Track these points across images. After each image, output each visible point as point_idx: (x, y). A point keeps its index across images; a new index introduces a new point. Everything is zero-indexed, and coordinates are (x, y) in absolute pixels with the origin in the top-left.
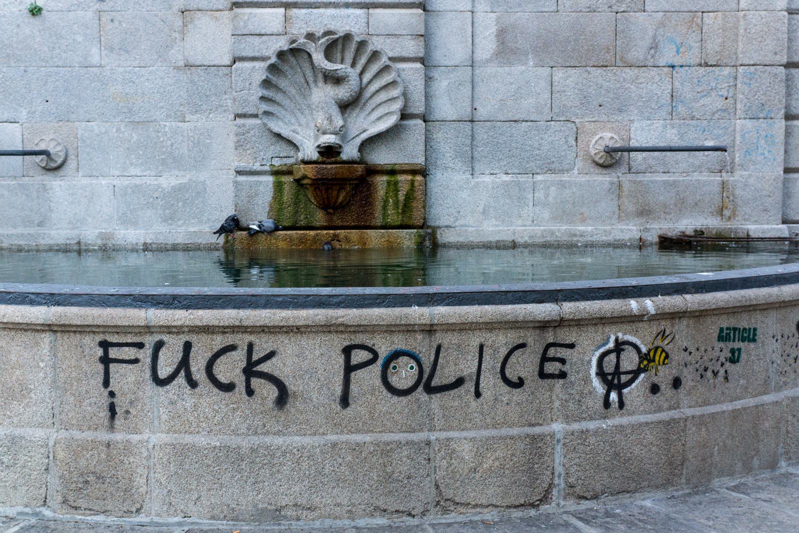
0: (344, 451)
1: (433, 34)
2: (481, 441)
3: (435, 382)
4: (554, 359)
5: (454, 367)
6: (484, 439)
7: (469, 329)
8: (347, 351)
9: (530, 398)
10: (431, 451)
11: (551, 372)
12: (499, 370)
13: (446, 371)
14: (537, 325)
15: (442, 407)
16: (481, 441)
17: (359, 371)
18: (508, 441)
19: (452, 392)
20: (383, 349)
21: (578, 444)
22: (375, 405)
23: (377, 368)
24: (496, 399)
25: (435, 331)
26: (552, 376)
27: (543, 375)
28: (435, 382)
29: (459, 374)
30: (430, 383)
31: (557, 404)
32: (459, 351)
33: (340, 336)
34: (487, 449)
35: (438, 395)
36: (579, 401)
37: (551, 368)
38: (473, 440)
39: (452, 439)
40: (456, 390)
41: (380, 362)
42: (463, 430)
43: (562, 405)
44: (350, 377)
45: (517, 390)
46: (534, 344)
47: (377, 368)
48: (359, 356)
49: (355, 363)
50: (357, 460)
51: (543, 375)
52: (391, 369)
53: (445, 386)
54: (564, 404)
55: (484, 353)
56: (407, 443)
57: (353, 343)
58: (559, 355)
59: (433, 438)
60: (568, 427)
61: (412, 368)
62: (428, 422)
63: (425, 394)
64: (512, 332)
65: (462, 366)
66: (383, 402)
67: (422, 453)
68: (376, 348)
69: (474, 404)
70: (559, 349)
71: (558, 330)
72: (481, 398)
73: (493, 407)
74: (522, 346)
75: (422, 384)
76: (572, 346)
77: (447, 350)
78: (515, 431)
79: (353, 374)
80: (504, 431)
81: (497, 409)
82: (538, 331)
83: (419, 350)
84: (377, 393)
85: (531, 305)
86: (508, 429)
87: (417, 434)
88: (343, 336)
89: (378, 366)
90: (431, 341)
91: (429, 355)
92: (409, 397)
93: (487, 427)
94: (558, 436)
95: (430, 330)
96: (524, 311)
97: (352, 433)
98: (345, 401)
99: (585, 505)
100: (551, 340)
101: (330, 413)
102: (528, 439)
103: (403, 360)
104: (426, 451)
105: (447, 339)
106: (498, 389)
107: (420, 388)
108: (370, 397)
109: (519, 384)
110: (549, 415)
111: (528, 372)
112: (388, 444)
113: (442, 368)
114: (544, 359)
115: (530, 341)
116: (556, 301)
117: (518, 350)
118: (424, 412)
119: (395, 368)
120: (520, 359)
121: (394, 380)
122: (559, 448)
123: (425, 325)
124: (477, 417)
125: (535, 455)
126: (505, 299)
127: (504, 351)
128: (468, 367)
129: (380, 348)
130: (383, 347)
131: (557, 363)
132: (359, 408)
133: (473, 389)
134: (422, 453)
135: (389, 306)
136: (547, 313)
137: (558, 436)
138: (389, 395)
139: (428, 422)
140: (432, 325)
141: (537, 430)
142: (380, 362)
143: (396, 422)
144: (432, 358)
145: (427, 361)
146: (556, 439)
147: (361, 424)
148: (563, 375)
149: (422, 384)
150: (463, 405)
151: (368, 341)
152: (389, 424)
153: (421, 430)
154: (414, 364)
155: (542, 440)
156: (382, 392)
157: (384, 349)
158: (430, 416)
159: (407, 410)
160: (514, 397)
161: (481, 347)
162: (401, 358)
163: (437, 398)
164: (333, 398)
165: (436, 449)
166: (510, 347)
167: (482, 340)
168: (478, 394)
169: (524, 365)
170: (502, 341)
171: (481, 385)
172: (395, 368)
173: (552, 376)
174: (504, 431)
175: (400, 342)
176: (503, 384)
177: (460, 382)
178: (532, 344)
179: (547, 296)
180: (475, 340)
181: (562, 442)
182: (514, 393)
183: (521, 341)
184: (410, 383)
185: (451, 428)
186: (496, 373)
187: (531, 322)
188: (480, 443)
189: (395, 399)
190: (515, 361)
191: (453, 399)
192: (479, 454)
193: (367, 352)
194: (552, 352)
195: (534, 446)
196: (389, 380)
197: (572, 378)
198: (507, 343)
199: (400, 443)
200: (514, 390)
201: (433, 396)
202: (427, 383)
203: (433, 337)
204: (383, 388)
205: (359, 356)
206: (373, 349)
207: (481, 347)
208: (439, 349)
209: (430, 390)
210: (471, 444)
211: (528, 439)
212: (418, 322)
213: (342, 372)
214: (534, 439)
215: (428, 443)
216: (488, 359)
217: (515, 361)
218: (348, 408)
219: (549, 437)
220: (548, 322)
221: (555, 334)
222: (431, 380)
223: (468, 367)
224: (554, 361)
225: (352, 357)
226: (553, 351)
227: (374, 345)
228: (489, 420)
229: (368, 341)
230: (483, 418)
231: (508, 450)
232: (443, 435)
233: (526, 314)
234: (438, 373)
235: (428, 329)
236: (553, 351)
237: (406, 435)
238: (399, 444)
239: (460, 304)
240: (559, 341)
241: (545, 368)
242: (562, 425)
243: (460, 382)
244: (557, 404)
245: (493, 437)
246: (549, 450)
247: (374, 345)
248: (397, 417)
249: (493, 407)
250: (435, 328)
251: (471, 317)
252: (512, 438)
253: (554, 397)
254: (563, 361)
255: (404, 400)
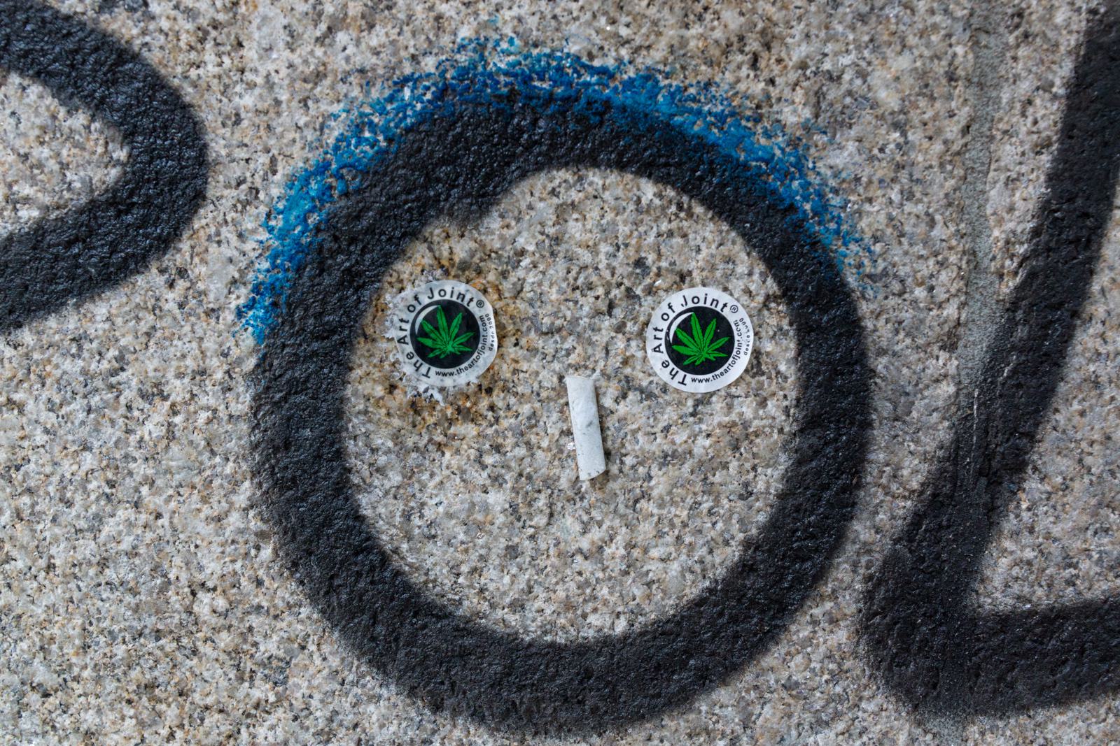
1: (94, 302)
20: (269, 53)
23: (187, 336)
41: (230, 246)
52: (385, 371)
75: (846, 585)
84: (212, 677)
91: (970, 159)
103: (574, 225)
107: (822, 637)
119: (448, 336)
121: (442, 513)
142: (230, 246)
149: (846, 585)
154: (738, 288)
156: (278, 670)
162: (536, 198)
184: (668, 560)
196: (378, 505)
204: (289, 619)
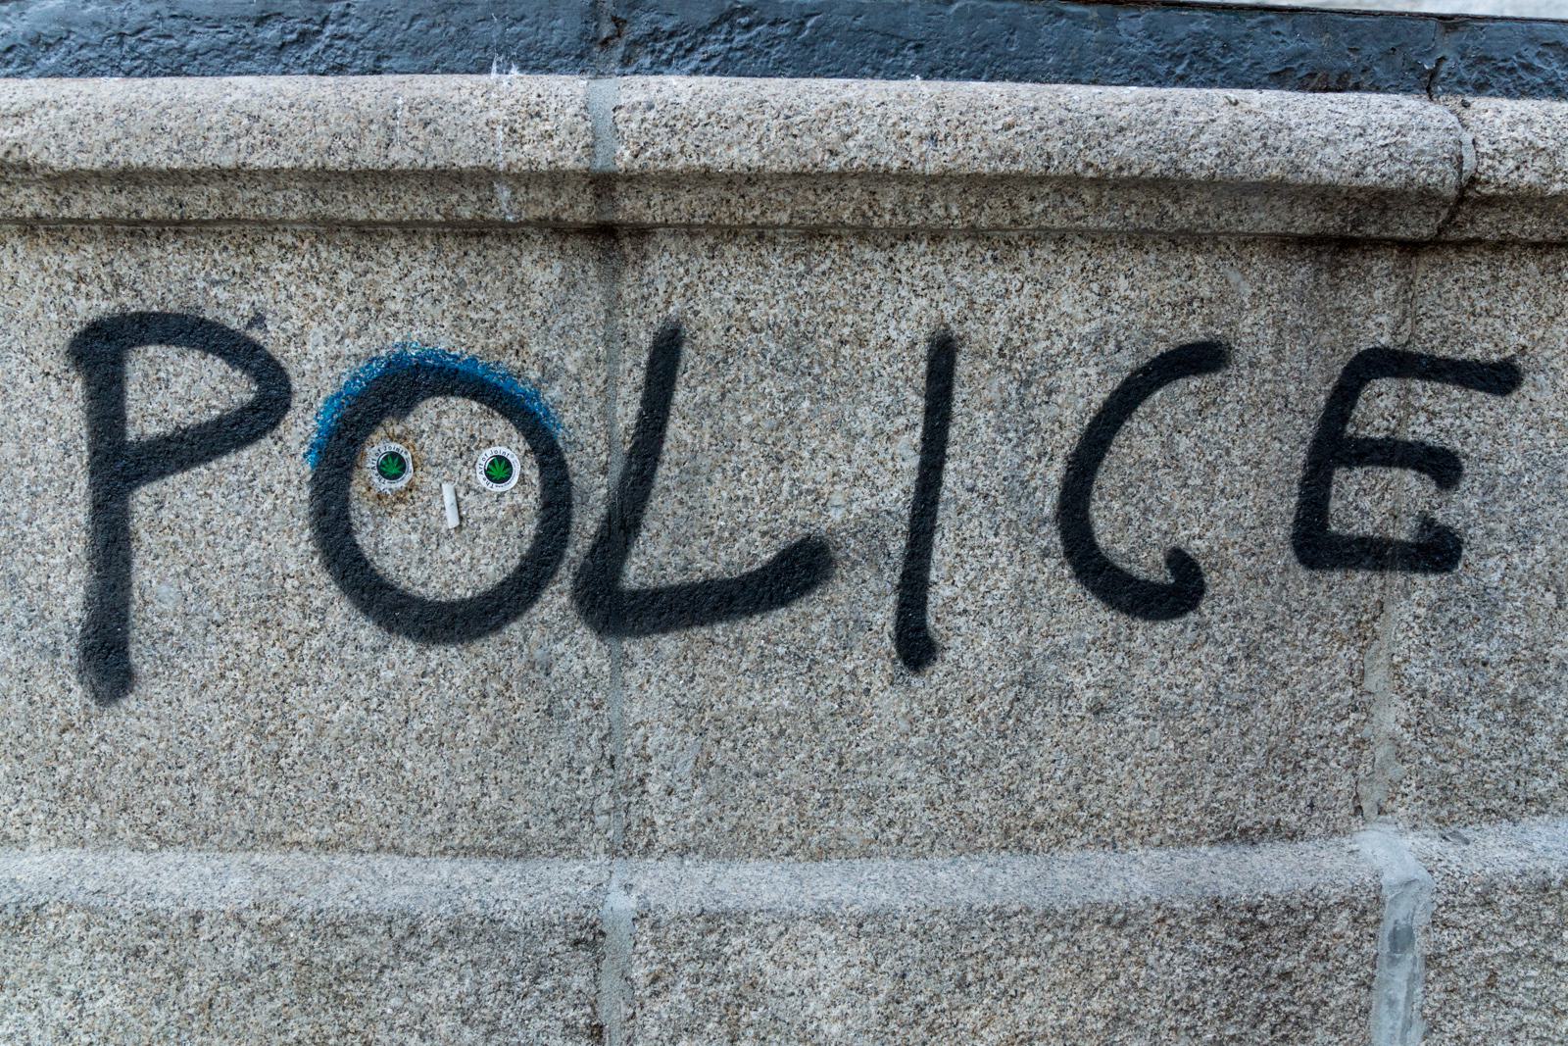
0: (76, 957)
2: (925, 933)
3: (647, 564)
4: (1393, 453)
5: (764, 476)
6: (942, 925)
7: (863, 233)
8: (101, 352)
9: (1237, 681)
10: (609, 982)
11: (1365, 528)
12: (1049, 504)
13: (716, 495)
14: (1305, 222)
15: (691, 715)
16: (925, 933)
17: (177, 479)
18: (1094, 938)
19: (756, 628)
21: (1514, 957)
22: (282, 691)
23: (283, 463)
24: (1026, 681)
25: (642, 232)
26: (1374, 553)
27: (1318, 544)
28: (647, 564)
29: (797, 521)
30: (617, 572)
31: (1391, 717)
32: (796, 372)
33: (52, 260)
34: (962, 985)
35: (669, 644)
36: (1520, 704)
37: (1370, 502)
38: (871, 925)
39: (741, 918)
40: (781, 616)
41: (300, 428)
42: (823, 854)
43: (1419, 724)
44: (125, 515)
45: (1163, 630)
46: (1278, 352)
47: (283, 463)
48: (173, 389)
49: (153, 429)
50: (160, 1016)
51: (1318, 544)
53: (709, 586)
54: (1432, 719)
55: (960, 393)
56: (456, 931)
57: (134, 306)
58: (1419, 430)
59: (622, 904)
60: (1452, 852)
61: (500, 469)
62: (605, 802)
63: (584, 635)
64: (1142, 265)
65: (816, 473)
66: (331, 672)
67: (550, 996)
68: (271, 338)
69: (891, 704)
70: (1423, 391)
71: (1426, 272)
72: (938, 671)
73: (1011, 724)
74: (1201, 358)
76: (1500, 378)
77: (719, 365)
78: (1137, 875)
79: (142, 499)
80: (1080, 875)
81: (1036, 738)
82: (1303, 273)
83: (544, 362)
84: (292, 617)
85: (1271, 95)
86: (1098, 857)
87: (539, 868)
88: (72, 263)
89: (287, 453)
90: (613, 306)
92: (489, 649)
93: (969, 841)
94: (1396, 914)
95: (602, 219)
96: (1225, 117)
97: (163, 843)
98: (107, 656)
99: (698, 56)
100: (1379, 333)
101: (30, 726)
102: (1215, 931)
103: (445, 418)
104: (578, 981)
105: (723, 296)
106: (1039, 619)
107: (556, 600)
108: (251, 643)
109: (1176, 591)
110: (1344, 784)
111: (1233, 523)
112: (336, 930)
113: (691, 476)
114: (1335, 447)
115: (1251, 330)
116: (1428, 84)
117: (1179, 386)
118: (579, 742)
120: (1183, 443)
121: (391, 544)
122: (1398, 979)
123: (556, 179)
124: (911, 785)
125: (1259, 1018)
126: (1106, 47)
127: (1083, 390)
128: (857, 480)
129: (298, 338)
130: (316, 333)
131: (1410, 477)
132: (190, 704)
133: (884, 617)
134: (550, 996)
135: (339, 69)
136: (1379, 137)
137: (1396, 914)
138: (368, 633)
139: (605, 802)
140: (603, 183)
141: (1273, 871)
142: (300, 428)
143: (419, 797)
144: (628, 412)
145: (595, 428)
146: (1388, 926)
147: (208, 797)
148: (1437, 550)
150: (824, 706)
151: (222, 294)
152: (370, 801)
153: (567, 847)
154: (513, 448)
155: (1303, 934)
157: (321, 353)
158: (620, 769)
159: (475, 728)
160: (1142, 673)
161: (942, 355)
163: (660, 654)
164: (38, 635)
165: (640, 973)
166: (1127, 361)
167: (950, 311)
168: (916, 647)
169: (1208, 479)
170: (1073, 321)
171: (940, 593)
172: (393, 465)
173: (1374, 553)
174: (1080, 875)
175: (417, 306)
176: (1072, 587)
177: (800, 569)
178: (1265, 354)
179: (1371, 49)
180: (900, 303)
181: (1422, 945)
182: (1139, 643)
183: (1195, 330)
185: (746, 843)
186: (1035, 524)
187: (1271, 189)
188: (916, 949)
189: (404, 657)
190: (1153, 451)
191: (758, 670)
192: (907, 1010)
193: (217, 366)
194: (1381, 408)
195: (1254, 967)
196: (364, 540)
197: (1485, 567)
198: (1104, 333)
199: (413, 931)
200: (1140, 625)
201: (635, 648)
202: (596, 570)
203: (630, 276)
204: (325, 591)
205: (173, 389)
206: (255, 348)
207: (942, 355)
208: (667, 352)
209: (616, 609)
210: (858, 951)
211: (1215, 931)
212: (504, 156)
213: (83, 483)
214: (1254, 927)
215: (590, 938)
216: (986, 434)
217: (1153, 451)
218: (130, 702)
219: (1344, 917)
220: (1381, 200)
221: (1407, 296)
222: (623, 553)
223: (857, 480)
224: (1388, 463)
225: (132, 390)
226: (1387, 402)
227: (258, 320)
228: (980, 803)
229: (222, 294)
230: (948, 791)
231: (1091, 991)
232: (674, 885)
233: (1244, 137)
234: (663, 507)
235: (582, 211)
236: (1387, 402)
237: (469, 872)
238: (406, 934)
239: (803, 67)
240: (1430, 341)
241: (1335, 504)
242: (1411, 840)
243: (800, 569)
244: (1391, 717)
245: (1000, 915)
246: (1343, 991)
247: (258, 320)
248: (419, 765)
249: (1011, 724)
250: (629, 208)
251: (868, 130)
252: (1117, 920)
253: (1376, 680)
254: (1441, 467)
255: (459, 665)
